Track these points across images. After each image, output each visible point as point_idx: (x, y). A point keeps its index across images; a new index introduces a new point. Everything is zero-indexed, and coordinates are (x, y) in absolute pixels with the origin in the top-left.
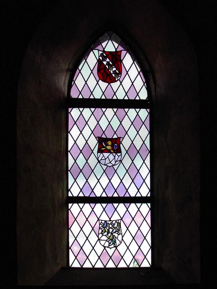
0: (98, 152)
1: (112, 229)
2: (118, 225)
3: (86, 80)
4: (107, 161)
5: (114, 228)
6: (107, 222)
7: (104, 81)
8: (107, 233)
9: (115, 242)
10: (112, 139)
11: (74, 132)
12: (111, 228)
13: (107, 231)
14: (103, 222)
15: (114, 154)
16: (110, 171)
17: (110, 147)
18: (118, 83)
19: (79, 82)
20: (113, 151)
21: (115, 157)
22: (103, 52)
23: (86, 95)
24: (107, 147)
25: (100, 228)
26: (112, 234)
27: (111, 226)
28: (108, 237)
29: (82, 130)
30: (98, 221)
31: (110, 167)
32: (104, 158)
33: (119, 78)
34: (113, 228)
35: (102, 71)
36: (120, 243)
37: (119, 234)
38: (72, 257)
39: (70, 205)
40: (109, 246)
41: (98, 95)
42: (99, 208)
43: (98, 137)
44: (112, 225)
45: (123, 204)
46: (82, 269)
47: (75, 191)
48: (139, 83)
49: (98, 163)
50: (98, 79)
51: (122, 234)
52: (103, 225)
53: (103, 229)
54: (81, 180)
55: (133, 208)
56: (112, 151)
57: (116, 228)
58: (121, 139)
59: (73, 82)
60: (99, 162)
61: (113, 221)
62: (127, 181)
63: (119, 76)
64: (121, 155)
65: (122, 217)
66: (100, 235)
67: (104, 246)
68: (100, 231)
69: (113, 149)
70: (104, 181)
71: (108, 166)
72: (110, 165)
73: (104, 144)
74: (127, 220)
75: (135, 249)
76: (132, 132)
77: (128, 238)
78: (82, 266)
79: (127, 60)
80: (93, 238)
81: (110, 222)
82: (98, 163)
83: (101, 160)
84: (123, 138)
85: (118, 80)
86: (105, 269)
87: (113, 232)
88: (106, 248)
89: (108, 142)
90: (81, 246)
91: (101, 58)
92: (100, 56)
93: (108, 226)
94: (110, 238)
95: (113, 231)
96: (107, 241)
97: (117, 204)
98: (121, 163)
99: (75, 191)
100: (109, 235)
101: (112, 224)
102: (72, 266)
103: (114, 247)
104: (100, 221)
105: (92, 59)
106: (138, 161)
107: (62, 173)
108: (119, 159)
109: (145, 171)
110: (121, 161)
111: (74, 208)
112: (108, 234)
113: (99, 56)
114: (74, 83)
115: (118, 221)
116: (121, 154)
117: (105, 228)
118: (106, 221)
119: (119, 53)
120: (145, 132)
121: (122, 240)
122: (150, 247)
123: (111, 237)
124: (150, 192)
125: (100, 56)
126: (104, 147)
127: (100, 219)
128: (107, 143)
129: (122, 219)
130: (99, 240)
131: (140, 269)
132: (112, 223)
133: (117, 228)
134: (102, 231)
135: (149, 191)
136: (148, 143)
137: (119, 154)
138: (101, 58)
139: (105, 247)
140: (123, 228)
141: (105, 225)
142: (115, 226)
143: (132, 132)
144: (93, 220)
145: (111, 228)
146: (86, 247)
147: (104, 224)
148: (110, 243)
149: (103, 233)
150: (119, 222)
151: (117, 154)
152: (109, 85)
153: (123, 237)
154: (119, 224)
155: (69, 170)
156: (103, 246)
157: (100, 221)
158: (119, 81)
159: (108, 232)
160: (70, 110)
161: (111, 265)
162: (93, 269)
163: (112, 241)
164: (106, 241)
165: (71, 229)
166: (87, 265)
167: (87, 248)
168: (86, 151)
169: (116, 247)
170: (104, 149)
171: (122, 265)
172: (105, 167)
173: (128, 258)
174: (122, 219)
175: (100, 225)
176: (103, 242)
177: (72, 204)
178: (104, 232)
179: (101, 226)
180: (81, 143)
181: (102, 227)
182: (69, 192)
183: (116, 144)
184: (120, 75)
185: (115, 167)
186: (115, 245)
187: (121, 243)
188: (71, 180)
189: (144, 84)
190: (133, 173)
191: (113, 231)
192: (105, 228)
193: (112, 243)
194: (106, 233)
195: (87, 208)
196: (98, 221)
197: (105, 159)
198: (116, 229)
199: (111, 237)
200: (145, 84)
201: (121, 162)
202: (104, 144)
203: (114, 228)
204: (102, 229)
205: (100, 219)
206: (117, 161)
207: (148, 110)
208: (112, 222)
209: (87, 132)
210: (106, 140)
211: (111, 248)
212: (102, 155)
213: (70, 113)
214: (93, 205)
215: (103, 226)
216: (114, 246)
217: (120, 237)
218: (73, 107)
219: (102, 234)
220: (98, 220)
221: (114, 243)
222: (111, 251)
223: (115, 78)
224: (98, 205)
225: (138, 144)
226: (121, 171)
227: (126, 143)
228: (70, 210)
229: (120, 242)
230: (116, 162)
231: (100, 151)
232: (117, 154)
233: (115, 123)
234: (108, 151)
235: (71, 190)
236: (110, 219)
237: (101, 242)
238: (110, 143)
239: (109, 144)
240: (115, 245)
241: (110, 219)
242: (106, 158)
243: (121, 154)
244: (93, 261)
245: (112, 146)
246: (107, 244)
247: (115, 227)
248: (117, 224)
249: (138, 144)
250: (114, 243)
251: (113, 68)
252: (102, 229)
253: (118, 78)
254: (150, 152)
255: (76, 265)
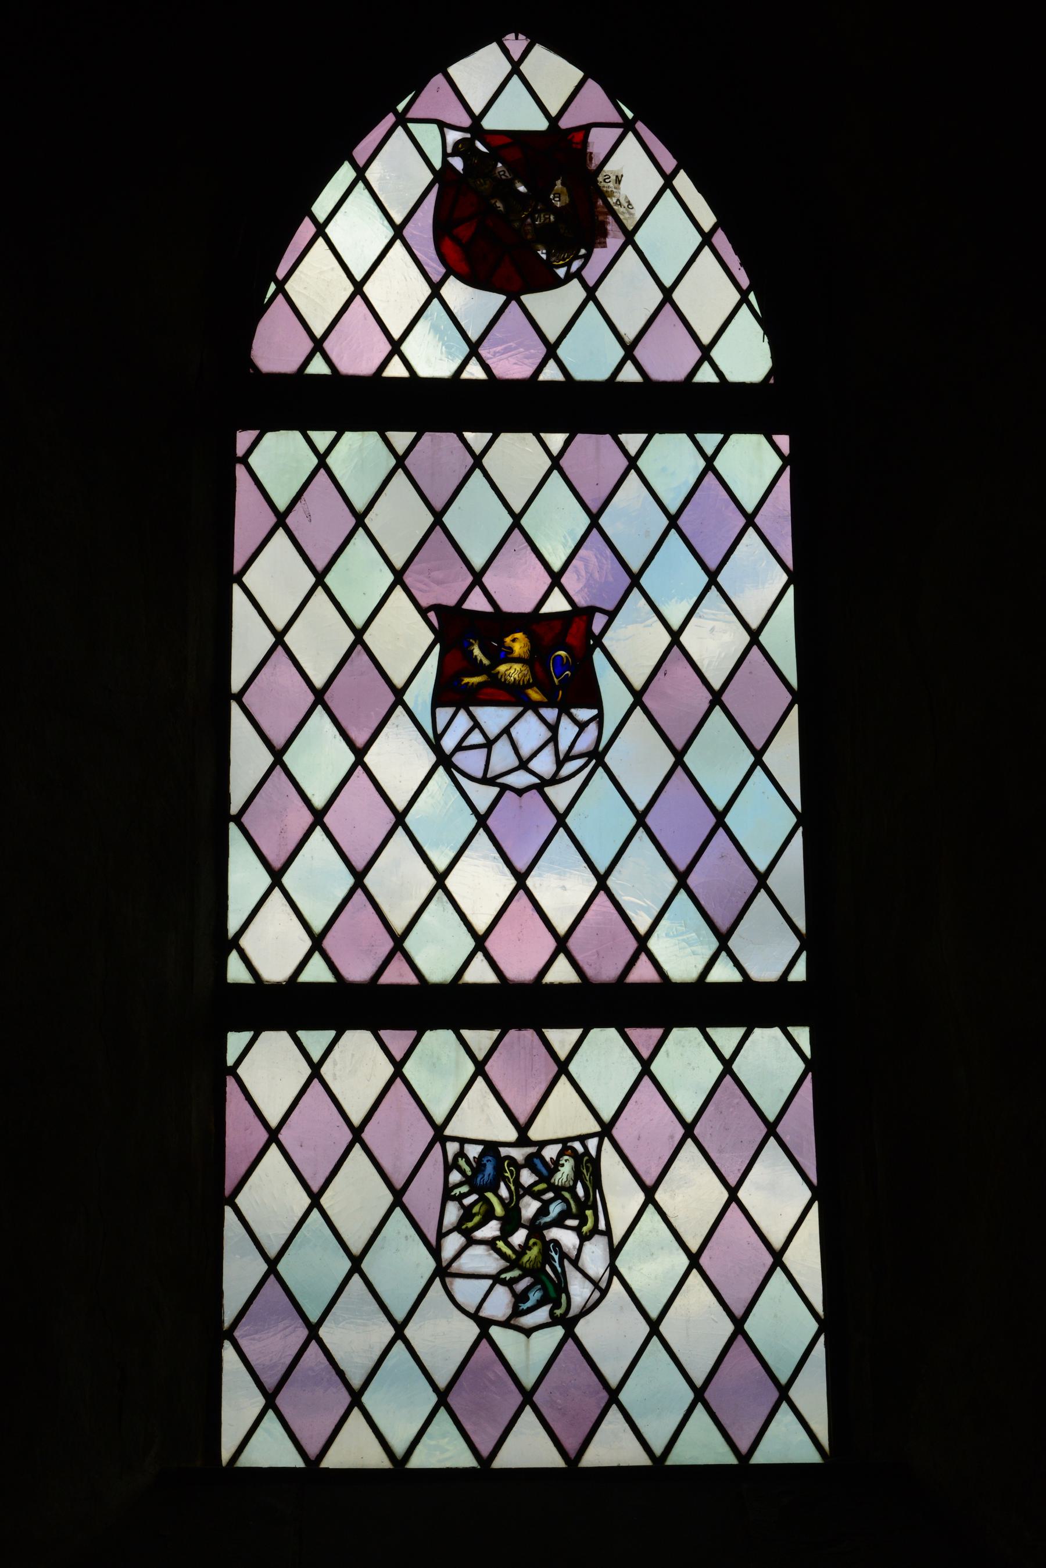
0: (438, 701)
1: (536, 1196)
2: (578, 1175)
3: (362, 270)
4: (502, 757)
5: (550, 1195)
6: (504, 1151)
7: (474, 280)
8: (501, 1230)
9: (562, 1287)
10: (532, 622)
11: (273, 577)
12: (529, 1191)
13: (499, 1210)
14: (473, 1151)
15: (551, 714)
16: (514, 812)
17: (517, 667)
18: (574, 292)
19: (313, 284)
20: (543, 692)
21: (554, 729)
22: (468, 136)
23: (357, 355)
24: (502, 668)
25: (447, 1194)
26: (536, 1229)
27: (527, 1178)
28: (509, 1252)
29: (323, 578)
30: (438, 1147)
31: (520, 792)
32: (476, 738)
33: (576, 265)
34: (544, 1192)
35: (465, 232)
36: (597, 1294)
37: (585, 1229)
38: (239, 1402)
39: (236, 1041)
40: (517, 1312)
41: (433, 357)
42: (439, 1061)
43: (437, 608)
44: (534, 1170)
45: (612, 1033)
46: (312, 1479)
47: (272, 948)
48: (712, 293)
49: (441, 769)
50: (436, 270)
51: (608, 1233)
52: (469, 1173)
53: (474, 1197)
54: (319, 877)
55: (687, 1060)
56: (535, 695)
57: (567, 1195)
58: (598, 622)
59: (273, 287)
60: (444, 761)
61: (543, 1144)
62: (643, 881)
63: (577, 257)
64: (599, 719)
65: (607, 1117)
66: (452, 1243)
67: (483, 1313)
68: (453, 1213)
69: (540, 680)
70: (481, 884)
71: (504, 788)
72: (520, 779)
73: (477, 651)
74: (647, 1129)
75: (710, 1275)
76: (675, 579)
77: (652, 1265)
78: (313, 1463)
79: (632, 170)
80: (401, 1263)
81: (519, 1154)
82: (441, 769)
83: (459, 747)
84: (612, 615)
85: (569, 277)
86: (484, 1480)
87: (547, 1219)
88: (495, 1331)
89: (508, 640)
90: (365, 776)
91: (458, 163)
92: (449, 150)
93: (506, 1181)
94: (525, 1259)
95: (548, 1213)
96: (504, 1283)
97: (575, 1033)
98: (600, 770)
99: (272, 948)
100: (519, 1237)
101: (540, 1166)
102: (244, 1461)
103: (554, 1321)
104: (452, 1148)
105: (401, 166)
106: (719, 760)
107: (186, 822)
108: (586, 743)
109: (767, 821)
110: (597, 756)
111: (268, 1067)
112: (506, 1234)
113: (445, 155)
114: (281, 289)
115: (577, 1146)
116: (595, 712)
117: (490, 1195)
118: (491, 1147)
119: (578, 137)
120: (760, 579)
121: (614, 1271)
122: (793, 820)
123: (533, 1253)
124: (791, 590)
125: (453, 155)
126: (477, 668)
127: (448, 1132)
128: (502, 643)
129: (606, 1130)
130: (443, 1272)
131: (744, 1480)
132: (537, 1161)
133: (572, 1190)
134: (467, 1213)
135: (789, 698)
136: (782, 638)
137: (584, 714)
138: (458, 163)
139: (485, 1324)
140: (621, 1198)
141: (489, 1169)
142: (565, 1172)
143: (675, 579)
144: (400, 1138)
145: (529, 1191)
146: (342, 1298)
147: (478, 1166)
148: (520, 1298)
149: (470, 1225)
150: (587, 1151)
151: (574, 711)
152: (514, 303)
153: (615, 1252)
154: (589, 1168)
155: (234, 809)
156: (475, 1316)
157: (452, 1148)
158: (575, 281)
159: (511, 1221)
160: (248, 444)
161: (529, 1448)
162: (399, 1478)
163: (540, 1281)
164: (496, 1279)
165: (240, 1200)
166: (355, 1450)
167: (355, 1336)
168: (350, 697)
169: (569, 1323)
170: (479, 684)
171: (613, 1448)
172: (483, 796)
173: (657, 1398)
174: (606, 1130)
175: (448, 1169)
176: (468, 1292)
177: (247, 1035)
178: (476, 1219)
179: (455, 1177)
180: (319, 643)
181: (464, 1189)
182: (234, 959)
183: (562, 653)
184: (583, 252)
185: (560, 795)
186: (558, 1312)
187: (604, 1293)
188: (244, 877)
189: (744, 300)
190: (681, 822)
191: (543, 1211)
192: (490, 1195)
193: (535, 1296)
194: (491, 1229)
195: (358, 1063)
196: (438, 1147)
197: (489, 744)
198: (565, 1200)
199: (533, 1253)
200: (752, 297)
201: (601, 763)
202: (477, 651)
203: (550, 1195)
204: (467, 1201)
205: (448, 1132)
206: (569, 757)
207: (802, 1035)
208: (538, 1155)
209: (360, 577)
210: (499, 623)
211: (528, 1332)
212: (462, 722)
213: (244, 460)
214: (398, 1040)
215: (467, 1180)
216: (551, 1313)
217: (595, 1257)
218: (266, 425)
219: (467, 1234)
220: (440, 1136)
221: (552, 1294)
222: (529, 1352)
223: (549, 267)
224: (439, 1042)
225: (714, 643)
226: (600, 817)
227: (632, 643)
228: (233, 1071)
229: (595, 1283)
230: (560, 764)
231: (450, 693)
232: (574, 711)
233: (557, 524)
234: (512, 695)
235: (244, 942)
236: (523, 1129)
237: (459, 1286)
238: (519, 644)
239: (512, 658)
240: (558, 1312)
241: (523, 1129)
242: (492, 736)
243: (595, 712)
244: (400, 1426)
245: (534, 660)
246: (499, 1303)
247: (564, 1188)
248: (571, 1162)
249: (714, 643)
250: (552, 1294)
251: (535, 211)
252: (467, 1201)
253: (569, 265)
254: (798, 697)
255: (272, 1451)
